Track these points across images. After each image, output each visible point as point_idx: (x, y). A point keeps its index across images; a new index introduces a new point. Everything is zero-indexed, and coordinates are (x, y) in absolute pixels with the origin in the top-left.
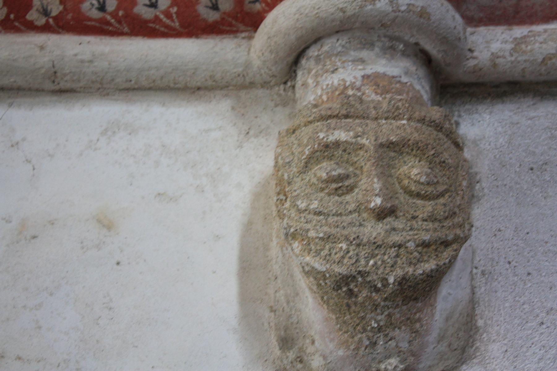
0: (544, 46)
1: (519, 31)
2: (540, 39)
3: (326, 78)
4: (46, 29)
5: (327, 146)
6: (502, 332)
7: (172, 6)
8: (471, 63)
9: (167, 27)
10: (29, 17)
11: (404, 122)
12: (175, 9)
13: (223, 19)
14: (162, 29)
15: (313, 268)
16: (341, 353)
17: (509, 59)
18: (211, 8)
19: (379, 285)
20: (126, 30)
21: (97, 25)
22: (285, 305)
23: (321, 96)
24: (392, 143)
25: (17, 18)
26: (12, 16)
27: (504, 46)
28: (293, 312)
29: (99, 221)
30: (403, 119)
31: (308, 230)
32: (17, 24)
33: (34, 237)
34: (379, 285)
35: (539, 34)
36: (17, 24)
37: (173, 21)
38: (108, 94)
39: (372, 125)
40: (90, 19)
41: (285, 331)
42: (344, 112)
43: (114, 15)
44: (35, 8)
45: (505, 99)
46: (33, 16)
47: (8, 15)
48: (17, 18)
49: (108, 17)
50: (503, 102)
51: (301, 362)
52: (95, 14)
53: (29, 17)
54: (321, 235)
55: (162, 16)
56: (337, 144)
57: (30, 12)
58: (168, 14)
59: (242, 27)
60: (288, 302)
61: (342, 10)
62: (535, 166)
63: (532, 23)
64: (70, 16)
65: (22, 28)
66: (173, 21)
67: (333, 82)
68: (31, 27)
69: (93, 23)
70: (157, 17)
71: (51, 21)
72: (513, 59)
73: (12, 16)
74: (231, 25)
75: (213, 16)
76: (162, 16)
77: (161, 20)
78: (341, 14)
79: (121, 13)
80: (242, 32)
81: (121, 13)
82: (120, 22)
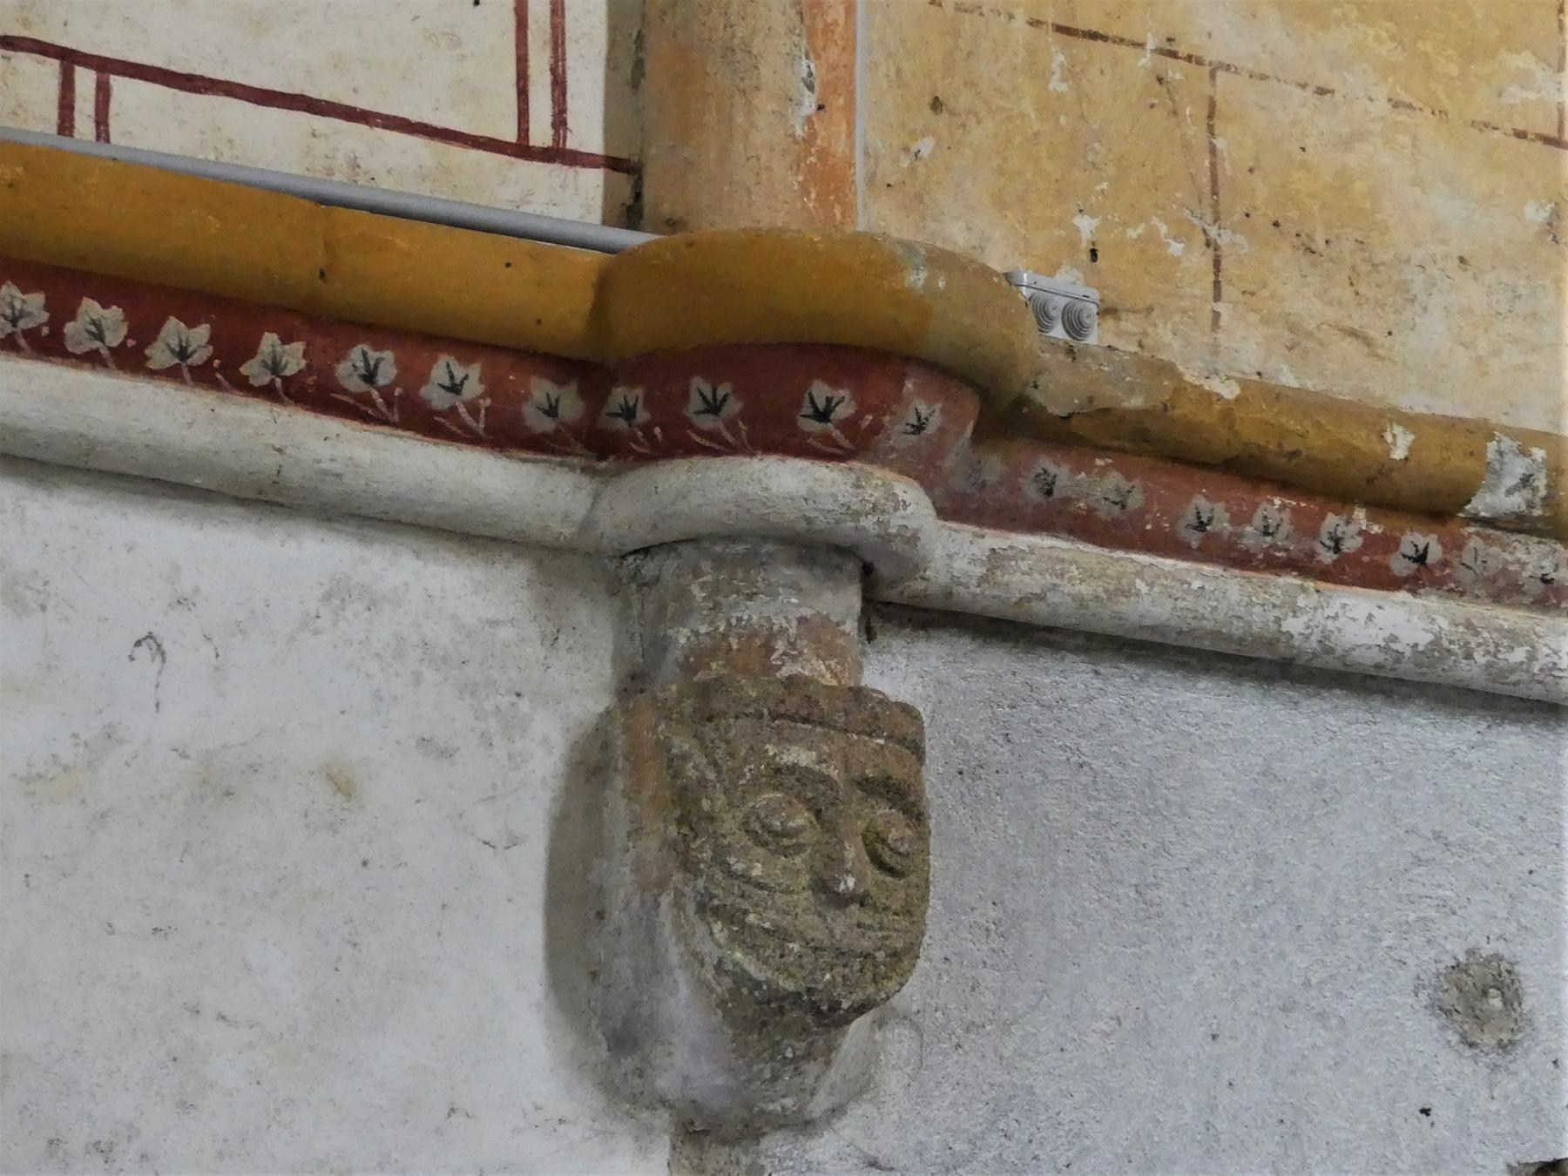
0: (1027, 579)
1: (995, 540)
2: (1024, 566)
3: (736, 603)
4: (267, 393)
5: (778, 771)
6: (905, 1053)
7: (482, 396)
8: (919, 586)
9: (464, 427)
10: (244, 370)
11: (882, 741)
12: (488, 402)
13: (557, 431)
14: (454, 429)
15: (744, 971)
16: (720, 1081)
17: (973, 589)
18: (545, 412)
19: (825, 1008)
20: (396, 418)
21: (351, 401)
22: (631, 984)
23: (725, 636)
24: (867, 780)
25: (221, 369)
26: (217, 363)
27: (971, 568)
28: (645, 998)
29: (330, 777)
30: (879, 737)
31: (746, 912)
32: (219, 376)
33: (228, 793)
34: (825, 1008)
35: (1021, 555)
36: (219, 376)
37: (477, 420)
38: (329, 519)
39: (840, 741)
40: (345, 392)
41: (625, 1024)
42: (804, 713)
43: (386, 392)
44: (259, 357)
45: (933, 633)
46: (252, 370)
47: (211, 360)
48: (221, 369)
49: (375, 394)
50: (928, 639)
51: (640, 1076)
52: (355, 384)
53: (244, 370)
54: (767, 925)
55: (462, 410)
56: (793, 769)
57: (251, 362)
58: (473, 409)
59: (579, 448)
60: (637, 980)
61: (809, 520)
62: (965, 768)
63: (1013, 529)
64: (310, 381)
65: (226, 384)
66: (477, 420)
67: (750, 618)
68: (244, 386)
69: (345, 398)
70: (453, 409)
71: (278, 381)
72: (978, 591)
73: (217, 363)
74: (566, 443)
75: (546, 425)
76: (462, 410)
77: (459, 414)
78: (804, 524)
79: (398, 392)
80: (576, 455)
81: (398, 392)
82: (389, 404)
